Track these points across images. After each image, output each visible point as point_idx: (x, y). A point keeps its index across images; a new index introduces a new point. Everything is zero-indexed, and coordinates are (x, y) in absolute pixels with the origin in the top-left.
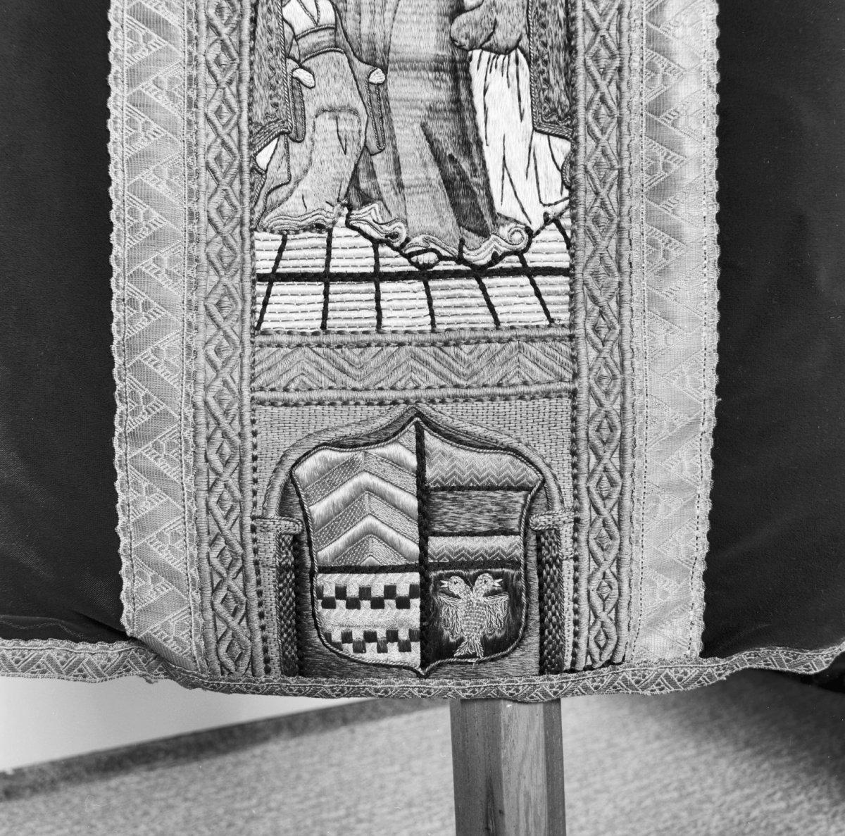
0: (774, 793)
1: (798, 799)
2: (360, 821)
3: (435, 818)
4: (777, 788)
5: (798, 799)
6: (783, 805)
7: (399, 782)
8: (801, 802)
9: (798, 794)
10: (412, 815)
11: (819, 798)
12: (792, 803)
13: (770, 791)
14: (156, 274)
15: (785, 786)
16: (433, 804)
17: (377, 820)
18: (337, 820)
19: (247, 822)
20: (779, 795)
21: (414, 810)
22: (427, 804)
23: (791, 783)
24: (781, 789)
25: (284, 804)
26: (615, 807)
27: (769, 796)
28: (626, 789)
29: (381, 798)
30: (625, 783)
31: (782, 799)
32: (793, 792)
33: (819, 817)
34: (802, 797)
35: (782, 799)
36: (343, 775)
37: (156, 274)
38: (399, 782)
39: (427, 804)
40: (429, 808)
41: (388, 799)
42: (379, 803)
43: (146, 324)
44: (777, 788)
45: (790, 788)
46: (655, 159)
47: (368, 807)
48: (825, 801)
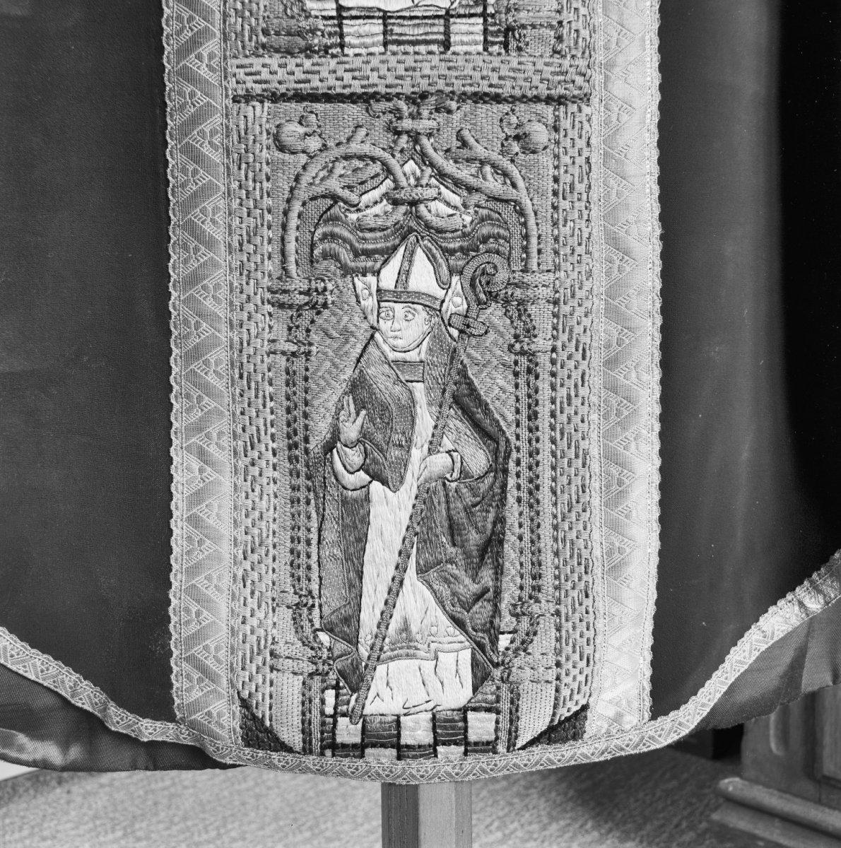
0: (491, 824)
1: (512, 827)
2: (185, 788)
3: (210, 828)
4: (494, 817)
5: (512, 827)
6: (499, 835)
7: (171, 796)
8: (516, 830)
9: (512, 822)
10: (188, 829)
11: (530, 823)
12: (507, 832)
13: (489, 820)
14: (204, 299)
15: (501, 814)
16: (207, 816)
17: (199, 785)
18: (164, 789)
19: (84, 798)
20: (496, 824)
21: (189, 823)
22: (202, 816)
23: (506, 810)
24: (499, 818)
25: (58, 831)
26: (370, 801)
27: (487, 827)
28: (356, 833)
29: (156, 814)
30: (357, 826)
31: (498, 828)
32: (507, 820)
33: (533, 791)
34: (516, 824)
35: (498, 828)
36: (116, 796)
37: (204, 299)
38: (171, 796)
39: (202, 816)
40: (204, 819)
41: (162, 815)
42: (154, 820)
43: (190, 35)
44: (494, 817)
45: (506, 815)
46: (612, 544)
47: (144, 825)
48: (535, 827)
